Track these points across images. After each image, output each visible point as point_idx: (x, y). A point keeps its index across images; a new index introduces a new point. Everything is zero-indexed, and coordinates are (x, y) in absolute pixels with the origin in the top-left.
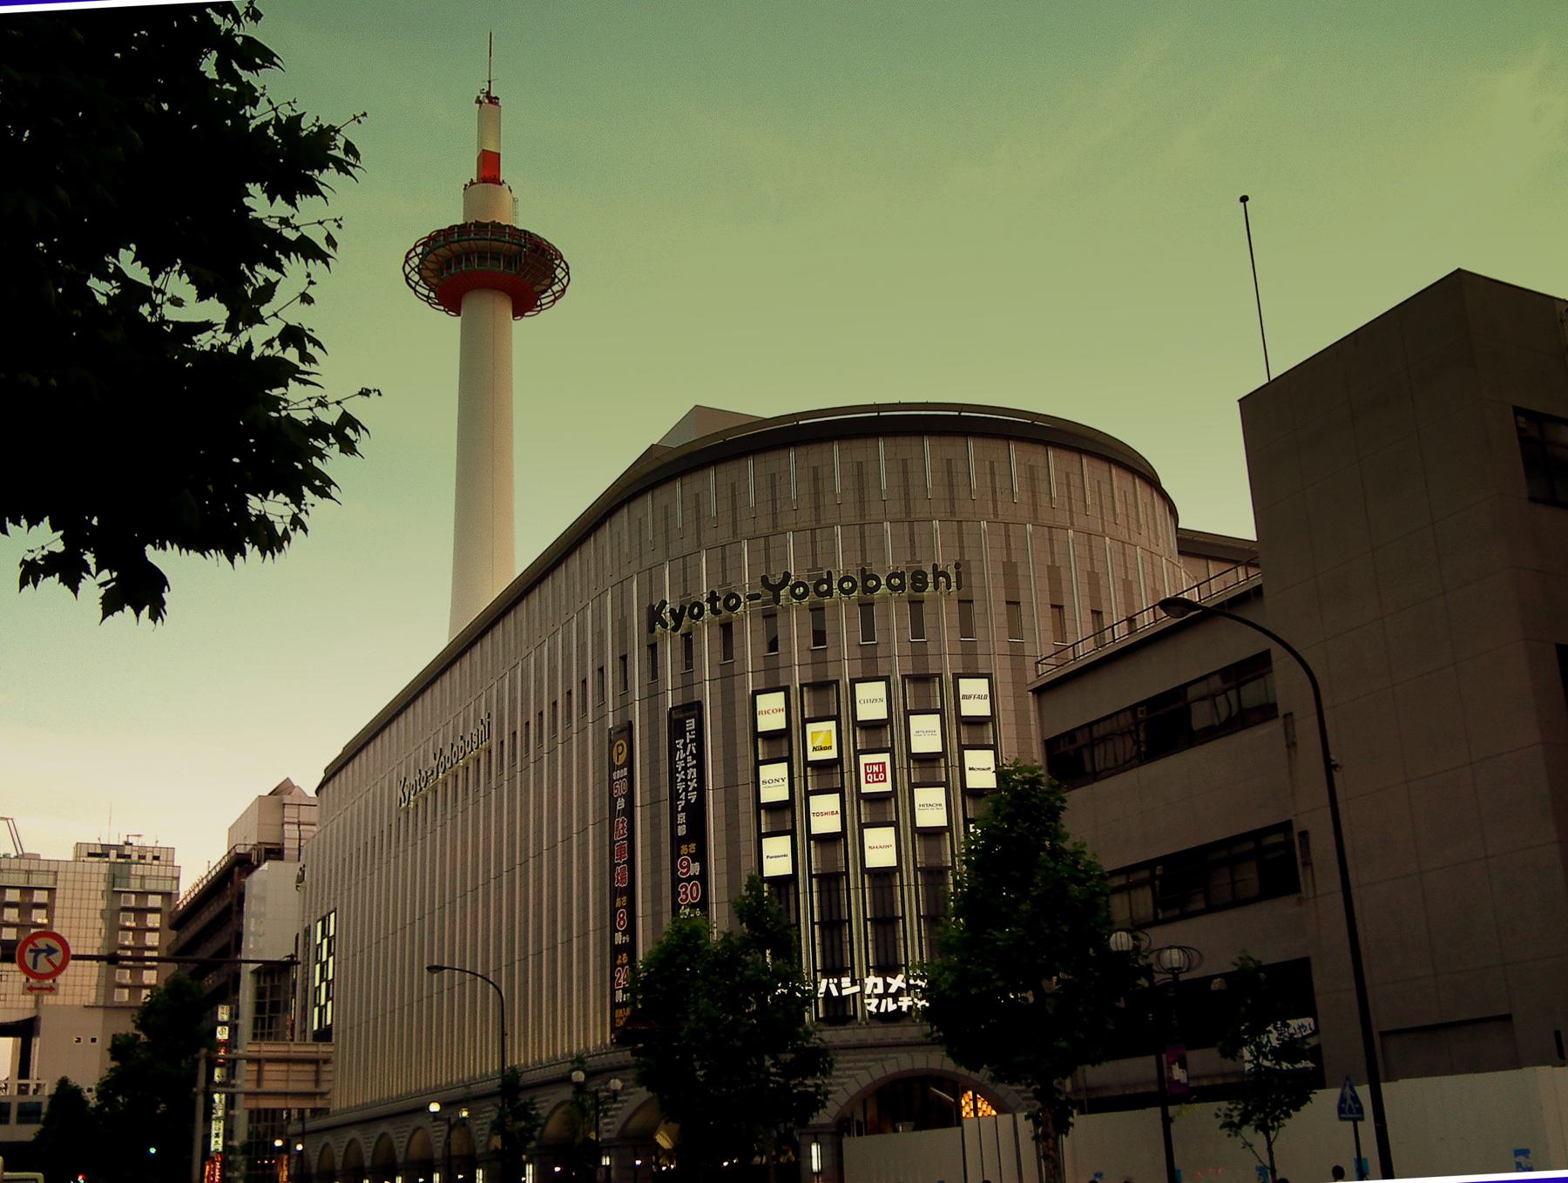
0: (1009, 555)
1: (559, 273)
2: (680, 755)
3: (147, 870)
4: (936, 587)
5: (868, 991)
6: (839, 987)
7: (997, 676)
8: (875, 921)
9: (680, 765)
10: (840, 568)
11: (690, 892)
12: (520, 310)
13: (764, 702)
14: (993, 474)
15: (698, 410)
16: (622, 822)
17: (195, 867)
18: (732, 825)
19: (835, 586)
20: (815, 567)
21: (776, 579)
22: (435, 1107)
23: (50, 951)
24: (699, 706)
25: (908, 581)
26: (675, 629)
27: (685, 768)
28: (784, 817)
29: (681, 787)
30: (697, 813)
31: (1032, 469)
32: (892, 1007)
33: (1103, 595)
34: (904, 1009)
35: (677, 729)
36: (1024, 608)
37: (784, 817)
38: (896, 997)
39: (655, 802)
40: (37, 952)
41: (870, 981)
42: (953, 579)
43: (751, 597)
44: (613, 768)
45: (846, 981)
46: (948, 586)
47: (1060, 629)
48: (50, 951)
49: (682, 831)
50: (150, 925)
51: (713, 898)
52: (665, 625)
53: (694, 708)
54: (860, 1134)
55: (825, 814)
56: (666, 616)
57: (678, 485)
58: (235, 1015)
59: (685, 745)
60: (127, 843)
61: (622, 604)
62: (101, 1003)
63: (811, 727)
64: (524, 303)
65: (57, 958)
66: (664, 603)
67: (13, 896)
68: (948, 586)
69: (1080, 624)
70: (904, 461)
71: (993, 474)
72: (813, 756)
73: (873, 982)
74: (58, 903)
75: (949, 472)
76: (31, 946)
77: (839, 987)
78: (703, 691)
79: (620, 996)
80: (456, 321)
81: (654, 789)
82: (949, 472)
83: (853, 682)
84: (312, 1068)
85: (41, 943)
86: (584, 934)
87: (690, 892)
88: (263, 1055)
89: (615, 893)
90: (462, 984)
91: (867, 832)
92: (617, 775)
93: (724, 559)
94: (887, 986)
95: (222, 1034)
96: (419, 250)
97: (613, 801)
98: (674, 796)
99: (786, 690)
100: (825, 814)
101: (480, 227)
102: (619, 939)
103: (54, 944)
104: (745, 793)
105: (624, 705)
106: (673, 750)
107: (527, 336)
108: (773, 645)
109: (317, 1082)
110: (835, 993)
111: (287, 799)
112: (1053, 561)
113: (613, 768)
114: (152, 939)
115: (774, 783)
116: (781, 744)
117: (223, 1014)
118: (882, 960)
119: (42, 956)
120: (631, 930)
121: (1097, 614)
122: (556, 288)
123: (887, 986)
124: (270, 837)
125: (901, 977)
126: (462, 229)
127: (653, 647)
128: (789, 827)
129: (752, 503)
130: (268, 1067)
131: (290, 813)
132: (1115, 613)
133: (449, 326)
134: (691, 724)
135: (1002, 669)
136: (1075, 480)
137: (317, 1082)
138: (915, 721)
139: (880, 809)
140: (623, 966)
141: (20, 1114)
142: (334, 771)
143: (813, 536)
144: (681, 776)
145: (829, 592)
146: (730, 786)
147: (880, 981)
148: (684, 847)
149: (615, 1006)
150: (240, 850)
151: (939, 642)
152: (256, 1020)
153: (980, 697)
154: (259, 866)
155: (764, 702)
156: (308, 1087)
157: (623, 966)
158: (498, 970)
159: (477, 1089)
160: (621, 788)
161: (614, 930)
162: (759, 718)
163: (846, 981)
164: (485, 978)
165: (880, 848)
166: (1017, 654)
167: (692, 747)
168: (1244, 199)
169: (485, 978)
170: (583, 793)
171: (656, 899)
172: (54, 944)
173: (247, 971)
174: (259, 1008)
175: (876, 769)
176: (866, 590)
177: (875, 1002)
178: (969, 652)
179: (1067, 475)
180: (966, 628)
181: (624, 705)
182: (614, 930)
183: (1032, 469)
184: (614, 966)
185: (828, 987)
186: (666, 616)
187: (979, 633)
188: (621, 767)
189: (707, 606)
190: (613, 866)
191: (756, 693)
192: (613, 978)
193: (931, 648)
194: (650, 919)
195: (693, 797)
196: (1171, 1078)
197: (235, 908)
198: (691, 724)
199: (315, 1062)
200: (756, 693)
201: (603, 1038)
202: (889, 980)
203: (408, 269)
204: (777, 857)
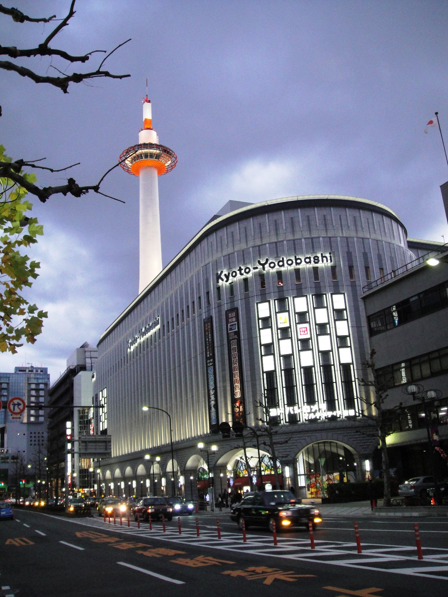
0: (348, 249)
4: (323, 261)
8: (313, 385)
14: (341, 220)
17: (56, 374)
19: (285, 262)
22: (201, 445)
23: (19, 404)
25: (312, 259)
26: (227, 281)
31: (355, 217)
33: (383, 262)
40: (14, 405)
42: (329, 258)
46: (327, 261)
47: (368, 276)
48: (19, 404)
50: (41, 395)
52: (223, 280)
56: (223, 276)
57: (225, 229)
58: (73, 425)
65: (21, 407)
67: (4, 386)
68: (327, 261)
69: (376, 274)
70: (308, 217)
71: (341, 220)
74: (10, 387)
75: (325, 220)
76: (12, 403)
82: (325, 220)
84: (104, 444)
85: (16, 402)
88: (87, 440)
94: (311, 409)
95: (69, 432)
103: (20, 402)
105: (209, 311)
111: (86, 349)
112: (365, 250)
114: (42, 399)
116: (267, 322)
117: (69, 424)
119: (16, 407)
121: (381, 269)
123: (311, 409)
124: (81, 363)
130: (89, 444)
131: (88, 354)
132: (388, 269)
135: (347, 289)
136: (370, 221)
137: (106, 449)
143: (276, 245)
145: (283, 265)
150: (71, 367)
151: (324, 281)
154: (78, 373)
159: (164, 450)
166: (353, 286)
168: (436, 113)
172: (20, 402)
173: (76, 410)
175: (304, 329)
176: (297, 264)
179: (368, 219)
181: (209, 311)
183: (355, 217)
189: (238, 272)
193: (322, 284)
196: (433, 439)
199: (105, 442)
204: (268, 363)
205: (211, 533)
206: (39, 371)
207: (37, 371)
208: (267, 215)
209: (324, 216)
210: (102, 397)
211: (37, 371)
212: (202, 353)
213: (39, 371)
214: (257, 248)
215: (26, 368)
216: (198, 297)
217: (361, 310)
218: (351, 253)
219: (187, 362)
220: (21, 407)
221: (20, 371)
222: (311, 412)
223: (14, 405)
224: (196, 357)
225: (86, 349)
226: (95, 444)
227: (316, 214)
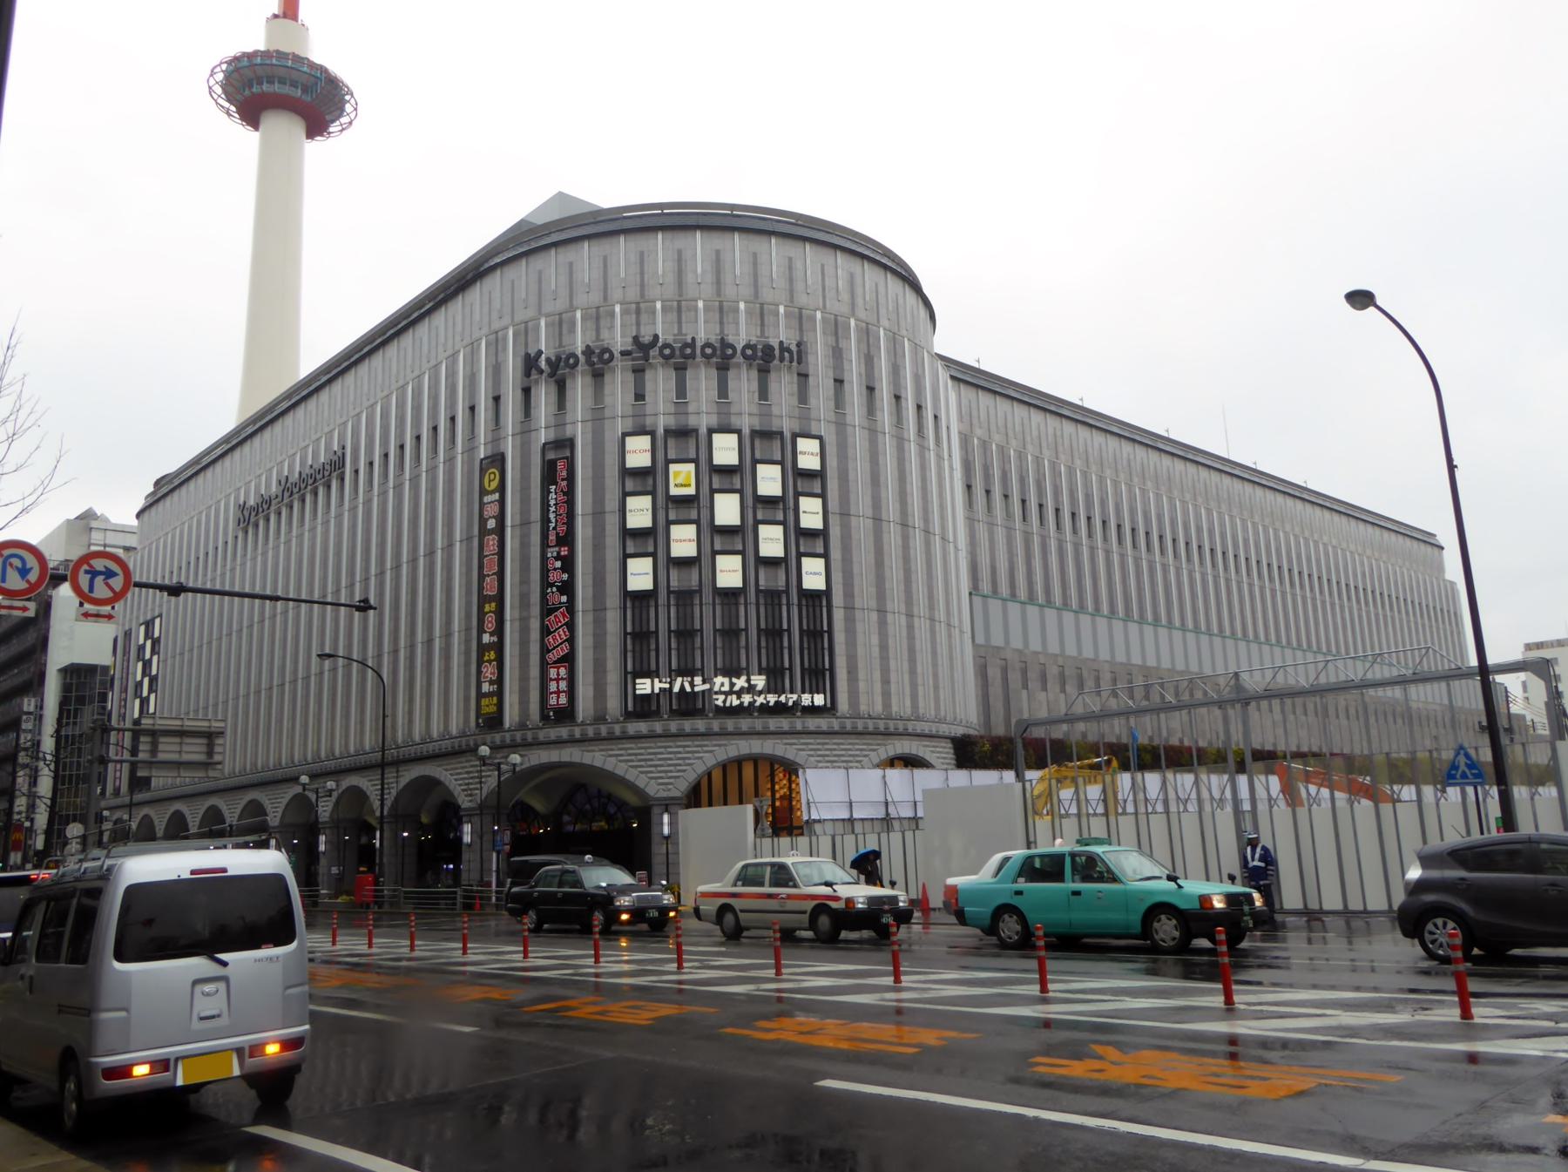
1: (348, 108)
5: (716, 688)
6: (692, 685)
7: (827, 439)
10: (701, 337)
12: (311, 134)
13: (719, 440)
15: (561, 197)
16: (492, 541)
18: (598, 546)
20: (680, 332)
21: (647, 339)
23: (109, 574)
24: (570, 443)
28: (648, 540)
32: (736, 702)
36: (846, 385)
37: (648, 540)
38: (739, 694)
39: (525, 523)
40: (94, 574)
41: (719, 680)
43: (623, 353)
44: (483, 492)
45: (698, 680)
46: (791, 361)
48: (109, 574)
54: (710, 805)
55: (683, 541)
56: (543, 364)
63: (673, 468)
64: (317, 126)
65: (117, 583)
66: (540, 353)
72: (674, 491)
73: (721, 682)
75: (790, 268)
76: (85, 567)
77: (692, 685)
79: (486, 688)
82: (790, 268)
83: (711, 431)
84: (204, 741)
85: (99, 564)
86: (447, 635)
89: (483, 600)
91: (718, 558)
92: (487, 499)
94: (732, 685)
96: (224, 67)
97: (483, 521)
99: (652, 434)
100: (683, 541)
101: (280, 55)
104: (612, 523)
107: (315, 150)
109: (210, 753)
110: (688, 689)
111: (94, 524)
115: (640, 512)
116: (646, 479)
119: (99, 580)
120: (499, 631)
122: (344, 120)
123: (732, 685)
125: (744, 678)
126: (266, 54)
127: (527, 391)
129: (622, 275)
133: (246, 140)
138: (761, 468)
139: (738, 538)
140: (490, 661)
145: (693, 356)
146: (598, 514)
147: (726, 680)
149: (480, 695)
155: (719, 440)
156: (202, 758)
157: (490, 661)
158: (379, 656)
161: (481, 631)
163: (698, 680)
164: (363, 663)
165: (729, 572)
177: (722, 697)
178: (805, 417)
180: (803, 397)
182: (481, 631)
185: (682, 686)
186: (543, 364)
187: (813, 401)
188: (493, 492)
191: (625, 435)
192: (479, 672)
194: (517, 624)
200: (625, 435)
201: (466, 720)
203: (212, 82)
204: (640, 574)
209: (790, 259)
210: (147, 637)
212: (469, 539)
216: (467, 405)
217: (608, 527)
219: (421, 560)
220: (117, 583)
222: (731, 692)
223: (94, 574)
224: (450, 546)
226: (177, 740)
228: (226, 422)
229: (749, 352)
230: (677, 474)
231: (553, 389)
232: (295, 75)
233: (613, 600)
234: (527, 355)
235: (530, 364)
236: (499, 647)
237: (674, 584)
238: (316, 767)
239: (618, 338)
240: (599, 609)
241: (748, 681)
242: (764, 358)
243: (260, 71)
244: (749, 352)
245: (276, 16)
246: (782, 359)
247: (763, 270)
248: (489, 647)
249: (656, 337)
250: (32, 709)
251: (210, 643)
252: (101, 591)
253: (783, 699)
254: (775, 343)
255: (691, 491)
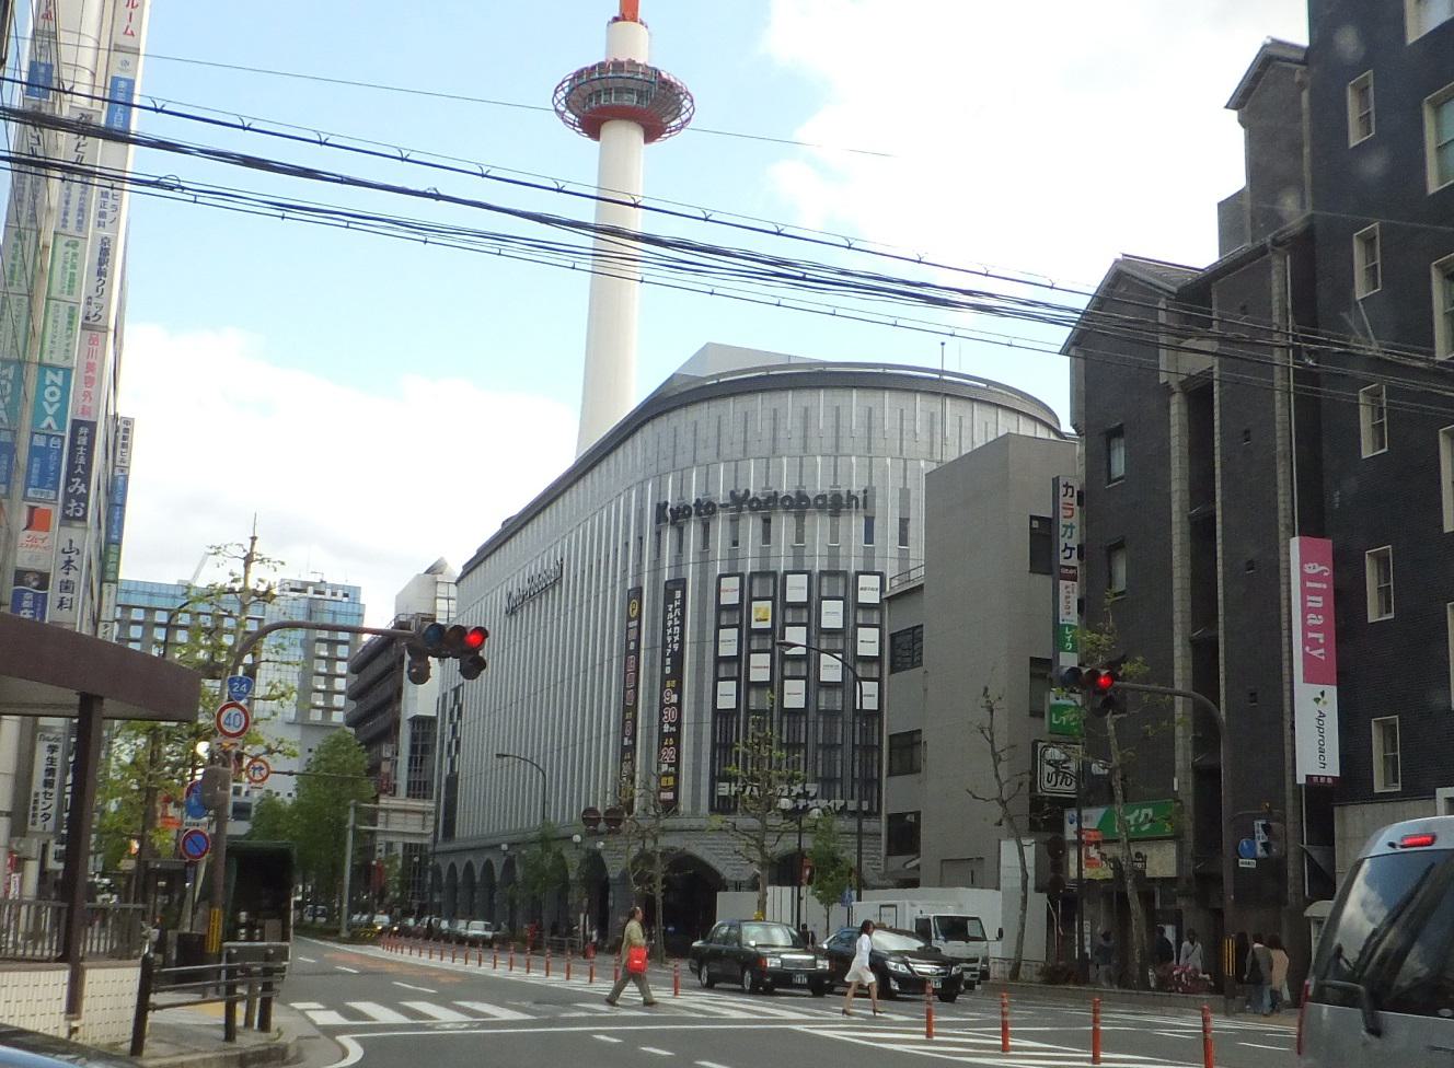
1: (686, 103)
2: (670, 616)
3: (337, 608)
9: (670, 623)
11: (670, 714)
18: (700, 670)
23: (261, 769)
27: (673, 626)
29: (669, 639)
30: (678, 659)
34: (801, 807)
35: (669, 598)
39: (653, 648)
40: (255, 769)
42: (861, 503)
48: (261, 769)
49: (668, 670)
51: (685, 719)
53: (680, 583)
59: (674, 609)
60: (322, 582)
61: (641, 500)
62: (299, 721)
63: (755, 604)
64: (653, 132)
65: (264, 772)
68: (857, 507)
72: (754, 625)
78: (688, 570)
80: (596, 144)
81: (653, 638)
84: (421, 816)
87: (670, 714)
90: (513, 764)
93: (707, 474)
98: (665, 645)
100: (760, 667)
101: (618, 65)
102: (627, 742)
103: (263, 766)
106: (666, 612)
108: (735, 543)
111: (439, 578)
113: (629, 619)
118: (826, 774)
119: (257, 772)
120: (634, 737)
123: (790, 791)
127: (658, 534)
128: (736, 674)
130: (393, 815)
131: (441, 590)
134: (678, 594)
136: (966, 423)
141: (234, 811)
142: (471, 567)
144: (669, 631)
146: (700, 642)
148: (668, 682)
150: (403, 619)
152: (411, 759)
153: (872, 589)
157: (627, 760)
158: (538, 756)
160: (633, 634)
162: (722, 594)
164: (537, 766)
167: (677, 611)
168: (943, 344)
169: (537, 766)
170: (612, 627)
171: (650, 717)
172: (263, 766)
174: (413, 749)
178: (869, 555)
180: (869, 538)
182: (624, 736)
184: (622, 761)
188: (633, 620)
190: (626, 689)
194: (645, 730)
195: (676, 647)
197: (398, 666)
198: (678, 594)
202: (793, 787)
204: (727, 696)
205: (1058, 1051)
206: (340, 593)
207: (334, 594)
208: (760, 397)
211: (334, 594)
213: (340, 593)
214: (733, 464)
215: (308, 584)
218: (909, 491)
221: (292, 590)
223: (255, 769)
224: (611, 660)
225: (439, 578)
227: (854, 402)
228: (565, 460)
229: (820, 502)
230: (758, 610)
231: (675, 533)
232: (631, 85)
233: (707, 717)
234: (658, 505)
235: (661, 508)
236: (677, 736)
237: (753, 705)
238: (513, 838)
239: (721, 495)
240: (698, 722)
241: (804, 788)
242: (836, 505)
243: (598, 86)
244: (820, 502)
245: (616, 19)
246: (849, 506)
247: (844, 422)
248: (669, 735)
249: (747, 492)
250: (389, 755)
251: (562, 681)
252: (258, 777)
253: (831, 804)
254: (843, 491)
255: (768, 625)
